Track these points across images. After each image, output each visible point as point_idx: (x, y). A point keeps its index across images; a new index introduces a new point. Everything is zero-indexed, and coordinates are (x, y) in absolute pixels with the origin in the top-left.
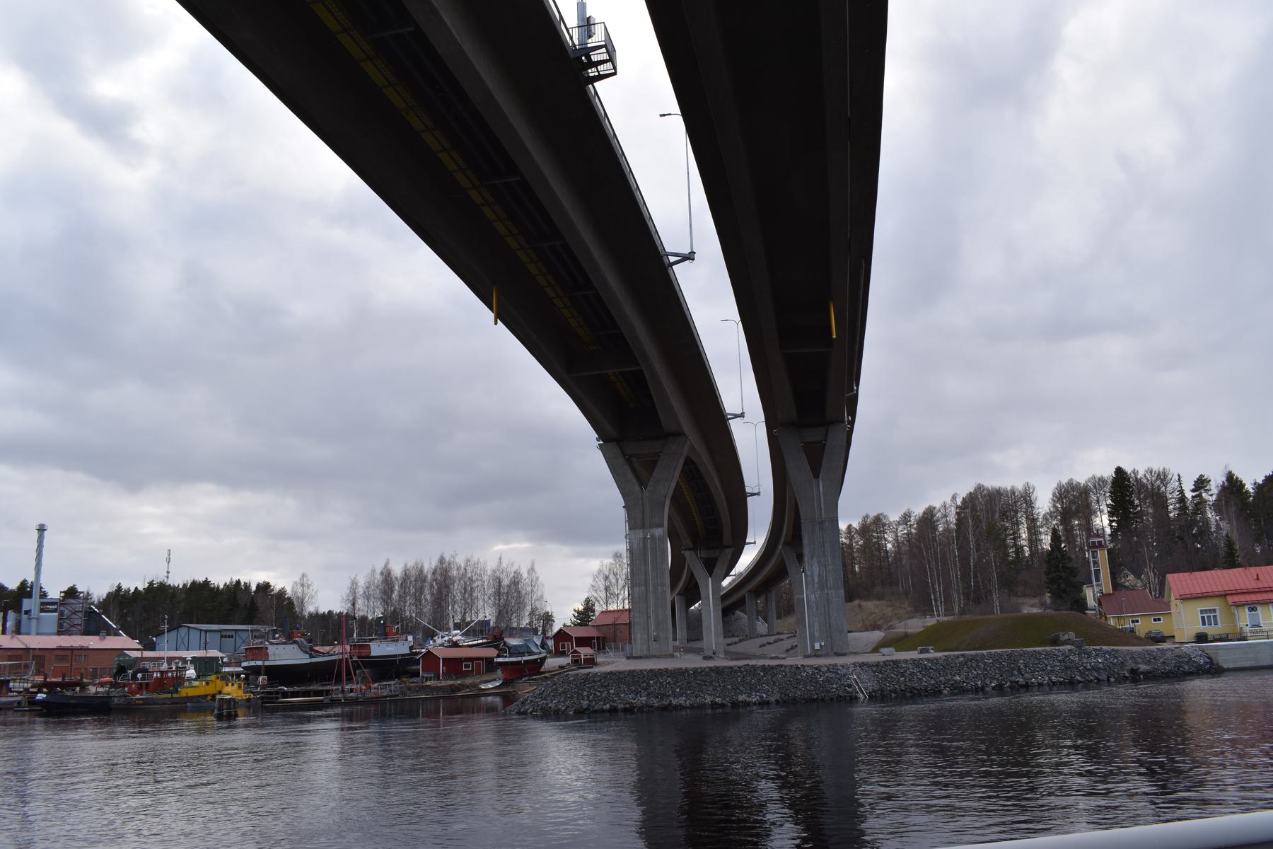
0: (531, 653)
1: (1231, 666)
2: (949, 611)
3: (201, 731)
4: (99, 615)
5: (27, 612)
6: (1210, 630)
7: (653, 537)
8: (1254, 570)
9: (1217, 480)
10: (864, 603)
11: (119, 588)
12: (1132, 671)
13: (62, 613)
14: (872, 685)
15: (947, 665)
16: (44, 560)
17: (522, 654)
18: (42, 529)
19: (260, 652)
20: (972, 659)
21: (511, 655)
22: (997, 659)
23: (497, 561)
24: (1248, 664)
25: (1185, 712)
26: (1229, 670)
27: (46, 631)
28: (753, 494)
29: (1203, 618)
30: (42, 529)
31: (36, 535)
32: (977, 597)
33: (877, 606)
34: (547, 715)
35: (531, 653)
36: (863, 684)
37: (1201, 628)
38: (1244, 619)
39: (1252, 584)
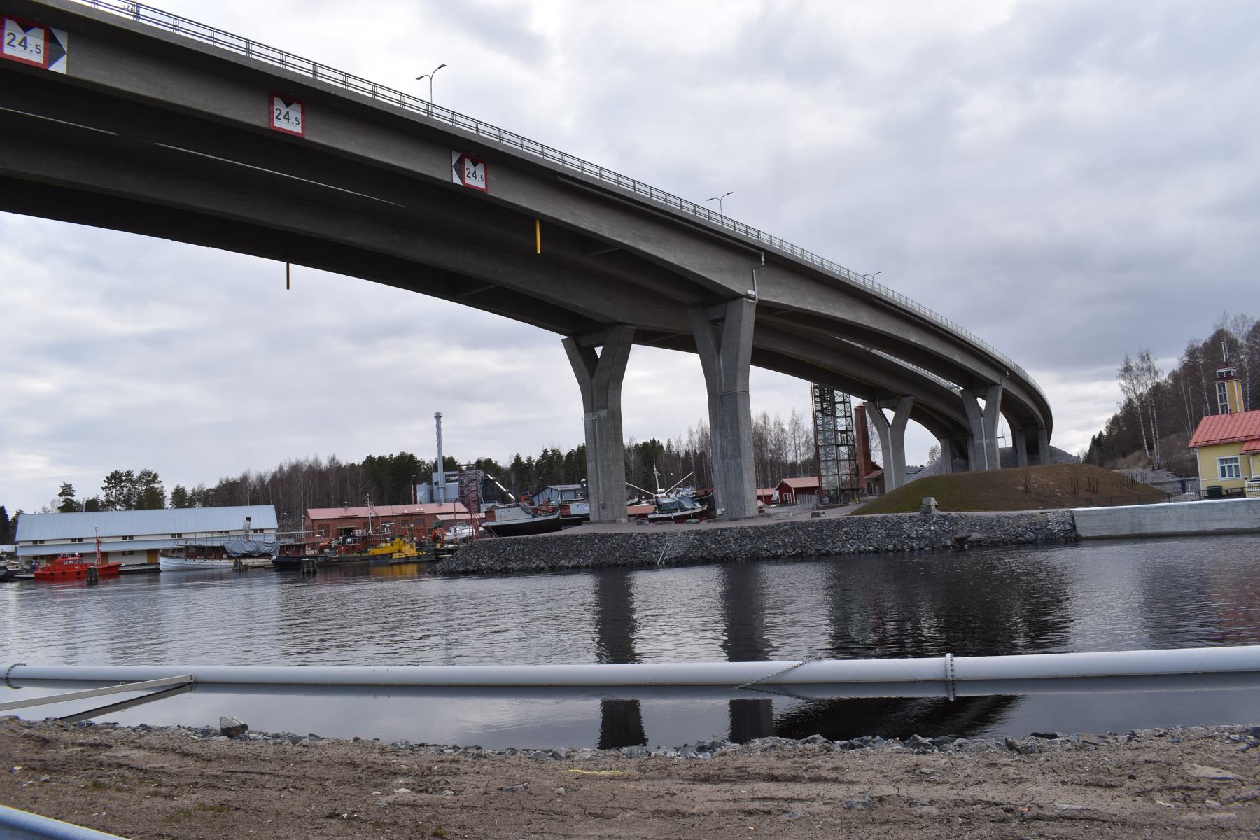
0: (683, 509)
1: (1089, 535)
3: (82, 587)
4: (493, 481)
5: (436, 483)
7: (599, 418)
11: (518, 459)
12: (961, 541)
13: (462, 483)
16: (443, 441)
17: (676, 510)
18: (438, 417)
19: (490, 515)
24: (1106, 533)
25: (830, 587)
26: (1087, 539)
29: (1223, 468)
30: (438, 417)
31: (434, 421)
34: (775, 559)
35: (683, 509)
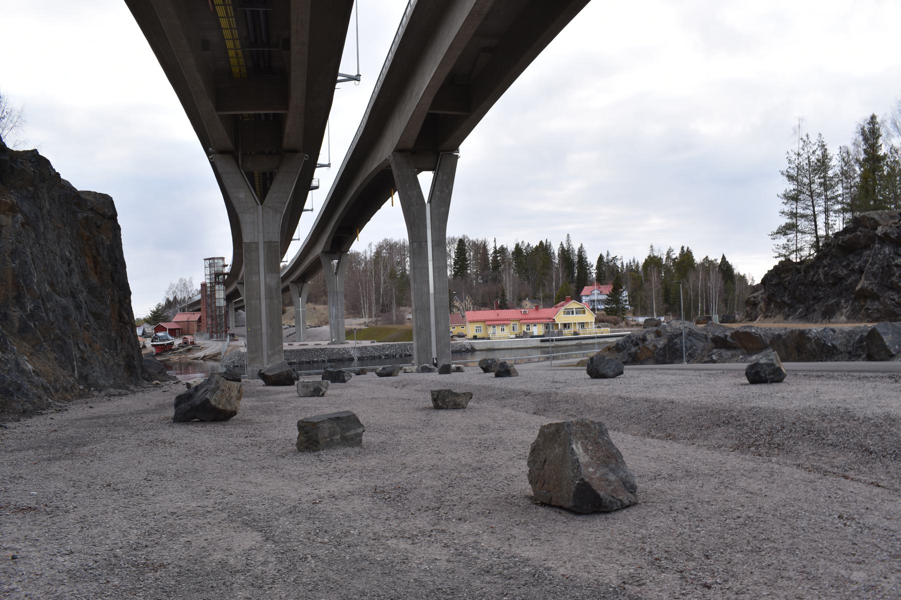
2: (370, 317)
6: (479, 335)
8: (498, 311)
9: (511, 248)
10: (317, 307)
14: (359, 355)
15: (383, 348)
17: (164, 340)
20: (392, 345)
21: (161, 341)
22: (400, 345)
23: (649, 249)
27: (245, 219)
28: (350, 78)
32: (384, 309)
33: (324, 309)
36: (356, 355)
37: (475, 334)
38: (491, 330)
39: (496, 318)
